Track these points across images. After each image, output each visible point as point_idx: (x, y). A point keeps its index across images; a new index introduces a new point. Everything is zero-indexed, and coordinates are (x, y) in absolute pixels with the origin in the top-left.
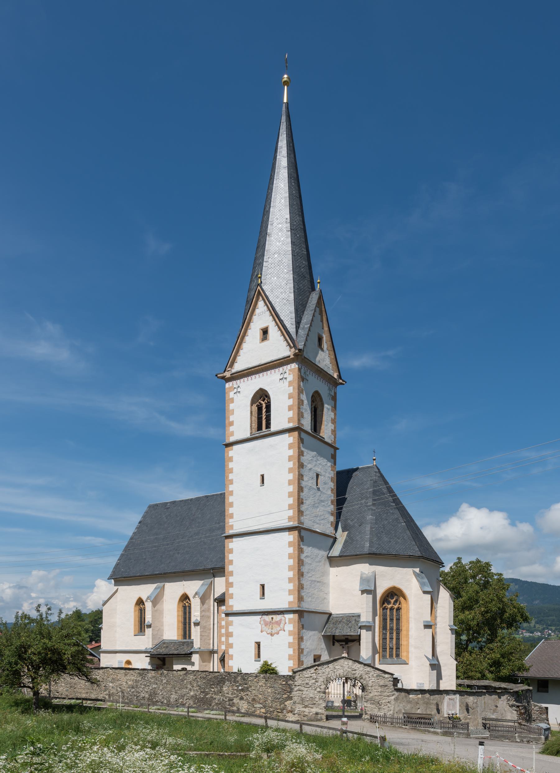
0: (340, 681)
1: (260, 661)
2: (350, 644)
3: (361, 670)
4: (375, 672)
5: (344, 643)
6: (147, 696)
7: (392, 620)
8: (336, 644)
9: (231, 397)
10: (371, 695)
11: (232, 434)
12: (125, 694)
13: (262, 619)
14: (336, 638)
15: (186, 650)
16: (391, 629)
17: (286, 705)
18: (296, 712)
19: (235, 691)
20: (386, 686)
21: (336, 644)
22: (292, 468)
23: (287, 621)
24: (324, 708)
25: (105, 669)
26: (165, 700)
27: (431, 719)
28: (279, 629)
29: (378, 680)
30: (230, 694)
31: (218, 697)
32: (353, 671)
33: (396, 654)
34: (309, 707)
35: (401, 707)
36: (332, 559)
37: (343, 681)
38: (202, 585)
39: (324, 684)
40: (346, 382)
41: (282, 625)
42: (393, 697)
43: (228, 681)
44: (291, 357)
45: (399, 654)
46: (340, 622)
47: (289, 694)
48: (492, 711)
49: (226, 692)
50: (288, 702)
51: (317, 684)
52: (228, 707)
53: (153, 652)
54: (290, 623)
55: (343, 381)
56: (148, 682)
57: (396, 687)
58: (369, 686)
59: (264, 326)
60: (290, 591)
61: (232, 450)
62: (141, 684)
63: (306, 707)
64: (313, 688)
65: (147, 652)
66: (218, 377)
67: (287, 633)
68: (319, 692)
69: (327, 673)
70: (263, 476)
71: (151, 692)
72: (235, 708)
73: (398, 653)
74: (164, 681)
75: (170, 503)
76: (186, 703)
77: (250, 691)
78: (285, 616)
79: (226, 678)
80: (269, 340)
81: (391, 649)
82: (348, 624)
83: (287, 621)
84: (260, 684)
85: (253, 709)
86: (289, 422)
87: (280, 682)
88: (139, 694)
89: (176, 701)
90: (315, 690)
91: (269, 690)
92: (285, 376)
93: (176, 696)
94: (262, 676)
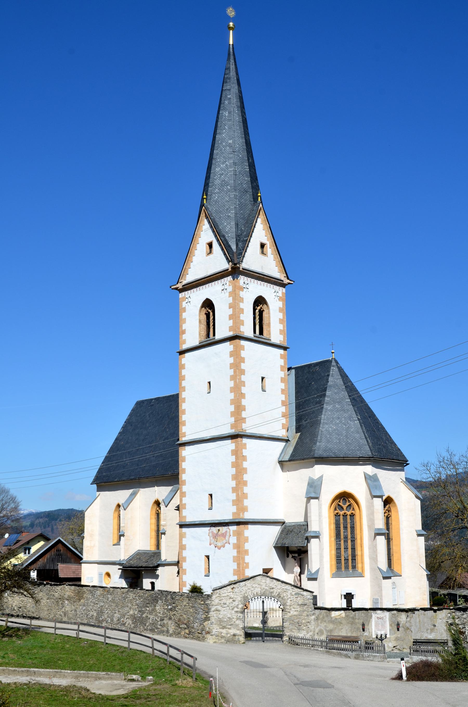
0: (259, 599)
1: (209, 576)
3: (279, 588)
4: (293, 590)
5: (296, 555)
6: (95, 614)
7: (345, 528)
10: (289, 615)
11: (184, 342)
12: (78, 612)
13: (210, 531)
14: (290, 549)
16: (346, 537)
17: (204, 626)
18: (213, 634)
20: (305, 605)
21: (290, 556)
24: (241, 629)
26: (110, 619)
27: (358, 642)
28: (225, 541)
29: (297, 599)
30: (161, 613)
31: (152, 616)
32: (271, 589)
33: (352, 566)
34: (227, 628)
35: (323, 627)
37: (262, 600)
38: (171, 491)
39: (242, 603)
41: (227, 537)
42: (313, 617)
43: (161, 600)
44: (229, 270)
45: (356, 566)
46: (291, 532)
47: (207, 614)
48: (429, 631)
49: (158, 611)
50: (206, 623)
51: (234, 603)
53: (125, 564)
55: (290, 280)
57: (316, 606)
58: (287, 605)
59: (209, 241)
60: (233, 501)
61: (184, 357)
62: (91, 602)
63: (224, 628)
64: (231, 608)
65: (120, 564)
66: (172, 289)
67: (231, 546)
69: (244, 592)
71: (98, 610)
72: (165, 629)
73: (355, 564)
74: (110, 599)
75: (155, 399)
76: (126, 622)
77: (177, 611)
78: (230, 527)
79: (159, 596)
80: (213, 254)
81: (346, 560)
84: (185, 603)
85: (179, 630)
86: (230, 331)
87: (200, 601)
88: (89, 612)
89: (118, 620)
90: (233, 609)
92: (226, 287)
93: (119, 615)
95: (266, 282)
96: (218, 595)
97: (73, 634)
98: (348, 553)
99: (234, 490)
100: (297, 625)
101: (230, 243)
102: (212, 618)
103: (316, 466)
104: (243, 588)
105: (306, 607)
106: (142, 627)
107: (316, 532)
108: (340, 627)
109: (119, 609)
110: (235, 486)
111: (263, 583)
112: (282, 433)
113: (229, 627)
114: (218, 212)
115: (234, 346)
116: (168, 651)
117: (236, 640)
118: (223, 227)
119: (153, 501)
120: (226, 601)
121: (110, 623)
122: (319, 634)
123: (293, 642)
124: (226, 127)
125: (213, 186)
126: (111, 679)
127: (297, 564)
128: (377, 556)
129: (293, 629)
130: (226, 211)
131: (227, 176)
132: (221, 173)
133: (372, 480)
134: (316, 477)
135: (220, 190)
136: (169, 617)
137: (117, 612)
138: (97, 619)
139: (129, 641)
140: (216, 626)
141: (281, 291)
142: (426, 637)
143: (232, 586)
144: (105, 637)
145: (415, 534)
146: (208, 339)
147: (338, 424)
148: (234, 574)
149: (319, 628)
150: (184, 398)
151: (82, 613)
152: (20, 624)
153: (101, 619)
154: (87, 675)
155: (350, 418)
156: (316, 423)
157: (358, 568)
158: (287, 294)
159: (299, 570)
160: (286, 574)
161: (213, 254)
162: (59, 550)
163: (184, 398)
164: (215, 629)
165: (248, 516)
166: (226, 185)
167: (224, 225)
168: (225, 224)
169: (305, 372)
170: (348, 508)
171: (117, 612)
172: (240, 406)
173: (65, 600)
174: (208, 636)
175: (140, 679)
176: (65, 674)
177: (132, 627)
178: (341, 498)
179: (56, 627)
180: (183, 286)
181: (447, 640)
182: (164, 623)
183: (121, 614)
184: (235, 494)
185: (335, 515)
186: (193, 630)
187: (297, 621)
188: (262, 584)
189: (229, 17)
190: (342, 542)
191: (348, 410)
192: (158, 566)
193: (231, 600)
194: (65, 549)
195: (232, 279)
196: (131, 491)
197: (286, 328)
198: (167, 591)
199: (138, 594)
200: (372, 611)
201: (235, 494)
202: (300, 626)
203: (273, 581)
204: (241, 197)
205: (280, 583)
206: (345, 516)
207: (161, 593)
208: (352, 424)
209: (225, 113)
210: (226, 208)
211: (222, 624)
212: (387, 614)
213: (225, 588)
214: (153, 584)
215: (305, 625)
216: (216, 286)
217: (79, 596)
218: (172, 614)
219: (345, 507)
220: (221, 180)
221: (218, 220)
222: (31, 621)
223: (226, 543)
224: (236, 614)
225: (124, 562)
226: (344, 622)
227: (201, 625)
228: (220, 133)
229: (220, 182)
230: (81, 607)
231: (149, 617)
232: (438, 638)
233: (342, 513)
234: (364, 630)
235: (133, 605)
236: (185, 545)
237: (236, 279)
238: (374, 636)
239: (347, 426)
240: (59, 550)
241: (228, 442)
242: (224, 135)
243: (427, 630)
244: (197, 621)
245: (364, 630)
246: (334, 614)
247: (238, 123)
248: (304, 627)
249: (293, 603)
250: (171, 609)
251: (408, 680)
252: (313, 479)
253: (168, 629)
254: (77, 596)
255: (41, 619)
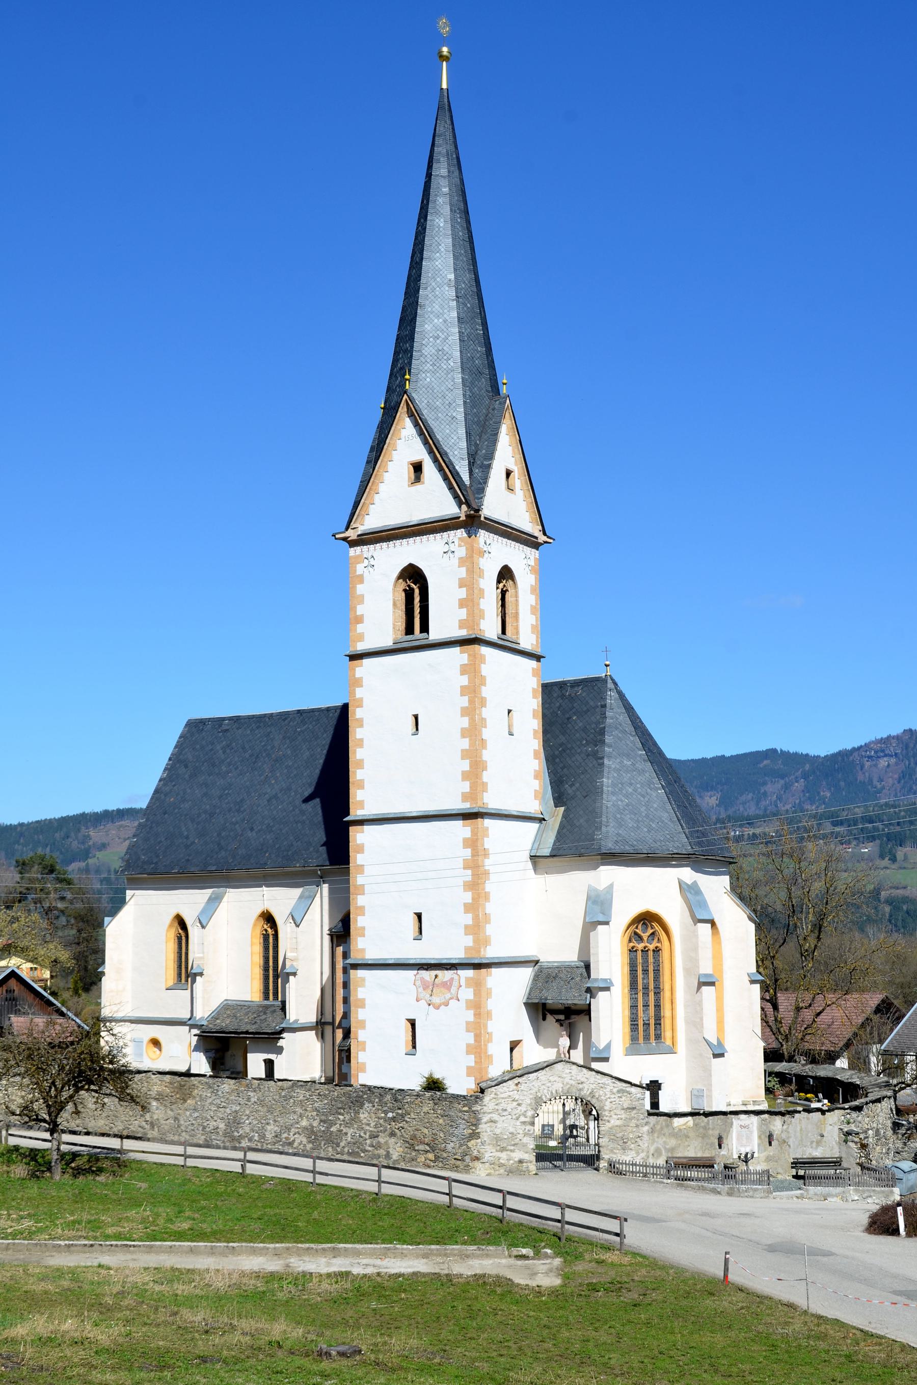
0: (558, 1101)
2: (574, 1018)
5: (562, 1017)
6: (222, 1126)
7: (646, 971)
8: (549, 1017)
9: (359, 572)
11: (361, 638)
12: (182, 1122)
14: (548, 1007)
15: (273, 1025)
16: (646, 988)
17: (468, 1148)
19: (381, 1121)
20: (634, 1108)
21: (549, 1017)
22: (467, 708)
23: (463, 982)
25: (144, 1074)
26: (257, 1135)
27: (713, 1167)
28: (448, 996)
30: (372, 1125)
31: (352, 1130)
36: (537, 859)
38: (301, 897)
40: (554, 540)
41: (453, 990)
42: (646, 1128)
43: (369, 1103)
44: (461, 519)
48: (814, 1144)
49: (365, 1121)
51: (520, 1108)
52: (370, 1149)
53: (207, 1026)
54: (468, 986)
55: (548, 537)
56: (222, 1100)
58: (605, 1110)
59: (416, 458)
60: (466, 927)
61: (361, 666)
62: (211, 1104)
63: (503, 1149)
64: (514, 1117)
67: (462, 1004)
68: (524, 1123)
69: (536, 1089)
70: (416, 717)
74: (253, 1100)
76: (294, 1141)
77: (407, 1122)
79: (365, 1096)
80: (423, 483)
81: (647, 1025)
82: (568, 983)
83: (463, 982)
86: (461, 627)
88: (208, 1122)
89: (276, 1136)
90: (517, 1119)
91: (441, 1121)
93: (276, 1128)
94: (428, 1094)
95: (513, 540)
96: (493, 1096)
97: (236, 1167)
98: (648, 1014)
99: (469, 908)
100: (621, 1142)
101: (457, 468)
102: (484, 1134)
103: (602, 868)
104: (534, 1083)
105: (635, 1112)
106: (330, 1149)
107: (605, 980)
108: (687, 1143)
109: (275, 1116)
110: (470, 901)
111: (566, 1074)
112: (533, 807)
113: (512, 1148)
114: (433, 408)
115: (469, 655)
116: (504, 1201)
117: (524, 1169)
118: (443, 437)
119: (259, 911)
120: (506, 1105)
121: (258, 1141)
122: (655, 1156)
123: (614, 1169)
124: (440, 247)
125: (421, 358)
126: (487, 1256)
127: (565, 1033)
128: (702, 1019)
129: (614, 1148)
130: (447, 407)
131: (447, 341)
132: (436, 335)
133: (693, 892)
134: (602, 886)
135: (435, 367)
136: (389, 1131)
137: (271, 1121)
138: (227, 1134)
139: (379, 1181)
140: (491, 1147)
141: (533, 554)
142: (810, 1154)
143: (516, 1081)
144: (314, 1172)
145: (747, 979)
146: (410, 637)
147: (631, 794)
148: (467, 1052)
149: (655, 1145)
150: (361, 740)
151: (192, 1124)
152: (81, 1145)
153: (236, 1134)
154: (443, 1252)
155: (649, 783)
156: (593, 792)
157: (665, 1039)
158: (541, 561)
159: (568, 1044)
160: (541, 1048)
161: (423, 483)
162: (10, 991)
163: (361, 740)
164: (489, 1153)
165: (491, 953)
166: (445, 358)
167: (445, 434)
168: (448, 431)
169: (555, 695)
170: (650, 939)
171: (271, 1121)
172: (480, 761)
173: (151, 1100)
174: (477, 1164)
175: (531, 1254)
176: (404, 1251)
177: (308, 1149)
178: (639, 922)
179: (187, 1153)
180: (359, 536)
181: (841, 1158)
182: (379, 1142)
183: (282, 1126)
184: (470, 916)
185: (630, 951)
186: (445, 1155)
187: (620, 1135)
188: (565, 1076)
189: (441, 34)
190: (640, 995)
191: (644, 771)
192: (283, 1030)
193: (515, 1104)
194: (22, 987)
195: (466, 535)
196: (208, 892)
197: (539, 623)
198: (382, 1088)
199: (318, 1091)
200: (733, 1116)
201: (470, 916)
202: (626, 1143)
203: (582, 1071)
204: (472, 383)
205: (594, 1073)
206: (645, 951)
207: (369, 1090)
208: (654, 794)
209: (437, 220)
210: (447, 402)
211: (500, 1143)
212: (754, 1119)
213: (504, 1084)
214: (269, 1064)
215: (633, 1141)
216: (433, 544)
217: (183, 1094)
218: (397, 1127)
219: (645, 936)
220: (436, 348)
221: (433, 422)
222: (122, 1146)
223: (451, 998)
224: (523, 1127)
225: (205, 1023)
226: (691, 1134)
227: (461, 1145)
228: (429, 258)
229: (433, 351)
230: (188, 1113)
231: (344, 1131)
232: (827, 1156)
233: (640, 946)
234: (720, 1146)
235: (306, 1110)
236: (364, 999)
237: (473, 536)
238: (736, 1156)
239: (646, 799)
240: (10, 991)
241: (458, 824)
242: (437, 263)
243: (812, 1142)
244: (454, 1139)
245: (720, 1146)
246: (677, 1122)
247: (461, 243)
248: (633, 1145)
249: (614, 1106)
250: (394, 1119)
251: (909, 1235)
252: (596, 890)
253: (388, 1152)
254: (177, 1093)
255: (148, 1140)
